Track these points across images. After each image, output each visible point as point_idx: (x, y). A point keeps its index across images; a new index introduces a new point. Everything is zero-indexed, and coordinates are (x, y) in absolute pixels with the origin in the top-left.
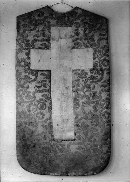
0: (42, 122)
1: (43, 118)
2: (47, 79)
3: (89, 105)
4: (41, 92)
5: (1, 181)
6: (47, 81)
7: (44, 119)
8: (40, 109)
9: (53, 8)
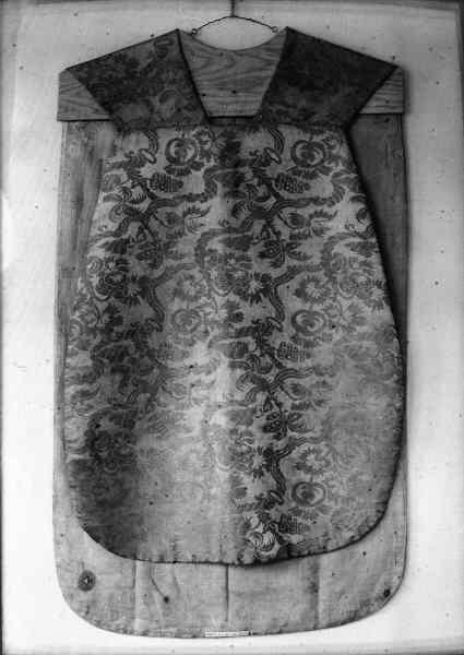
0: (304, 440)
1: (303, 284)
2: (288, 245)
3: (255, 154)
4: (311, 199)
5: (10, 642)
6: (288, 409)
7: (298, 278)
8: (316, 484)
9: (202, 37)
